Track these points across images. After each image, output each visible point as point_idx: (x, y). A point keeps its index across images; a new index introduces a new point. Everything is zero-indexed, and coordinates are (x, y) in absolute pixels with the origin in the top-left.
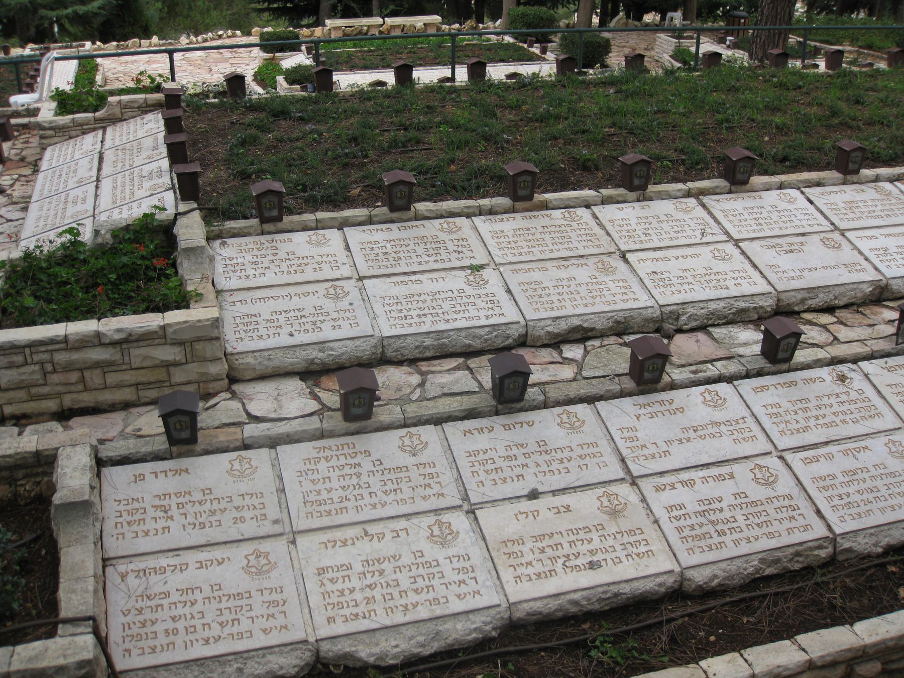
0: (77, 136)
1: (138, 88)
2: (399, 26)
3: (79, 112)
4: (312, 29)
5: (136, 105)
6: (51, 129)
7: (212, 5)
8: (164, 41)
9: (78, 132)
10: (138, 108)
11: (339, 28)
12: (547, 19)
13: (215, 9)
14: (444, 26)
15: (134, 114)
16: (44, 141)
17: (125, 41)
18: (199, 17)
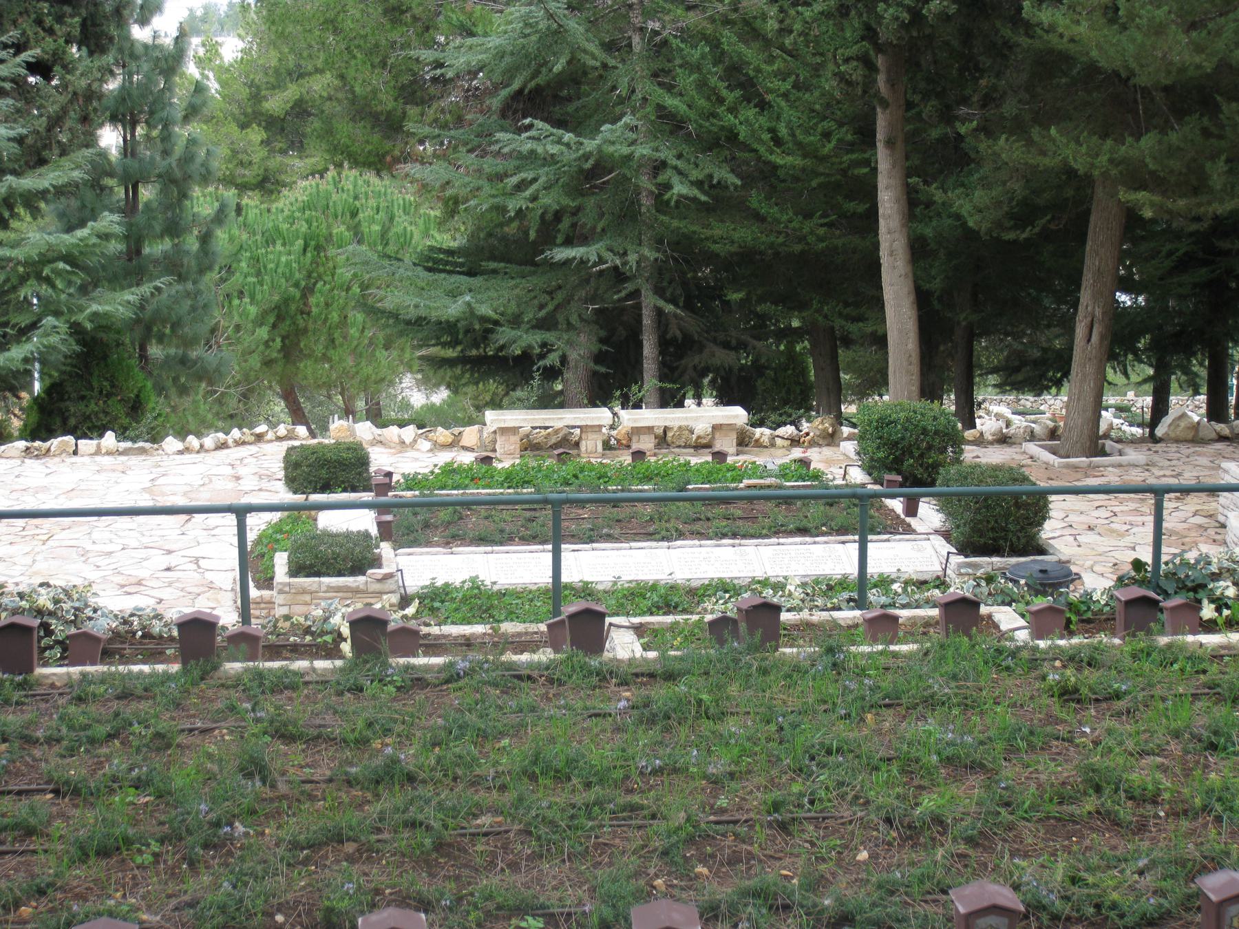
2: (650, 429)
3: (329, 575)
4: (456, 430)
7: (381, 336)
8: (129, 444)
11: (514, 430)
12: (936, 432)
13: (387, 347)
14: (758, 431)
17: (44, 440)
18: (350, 362)
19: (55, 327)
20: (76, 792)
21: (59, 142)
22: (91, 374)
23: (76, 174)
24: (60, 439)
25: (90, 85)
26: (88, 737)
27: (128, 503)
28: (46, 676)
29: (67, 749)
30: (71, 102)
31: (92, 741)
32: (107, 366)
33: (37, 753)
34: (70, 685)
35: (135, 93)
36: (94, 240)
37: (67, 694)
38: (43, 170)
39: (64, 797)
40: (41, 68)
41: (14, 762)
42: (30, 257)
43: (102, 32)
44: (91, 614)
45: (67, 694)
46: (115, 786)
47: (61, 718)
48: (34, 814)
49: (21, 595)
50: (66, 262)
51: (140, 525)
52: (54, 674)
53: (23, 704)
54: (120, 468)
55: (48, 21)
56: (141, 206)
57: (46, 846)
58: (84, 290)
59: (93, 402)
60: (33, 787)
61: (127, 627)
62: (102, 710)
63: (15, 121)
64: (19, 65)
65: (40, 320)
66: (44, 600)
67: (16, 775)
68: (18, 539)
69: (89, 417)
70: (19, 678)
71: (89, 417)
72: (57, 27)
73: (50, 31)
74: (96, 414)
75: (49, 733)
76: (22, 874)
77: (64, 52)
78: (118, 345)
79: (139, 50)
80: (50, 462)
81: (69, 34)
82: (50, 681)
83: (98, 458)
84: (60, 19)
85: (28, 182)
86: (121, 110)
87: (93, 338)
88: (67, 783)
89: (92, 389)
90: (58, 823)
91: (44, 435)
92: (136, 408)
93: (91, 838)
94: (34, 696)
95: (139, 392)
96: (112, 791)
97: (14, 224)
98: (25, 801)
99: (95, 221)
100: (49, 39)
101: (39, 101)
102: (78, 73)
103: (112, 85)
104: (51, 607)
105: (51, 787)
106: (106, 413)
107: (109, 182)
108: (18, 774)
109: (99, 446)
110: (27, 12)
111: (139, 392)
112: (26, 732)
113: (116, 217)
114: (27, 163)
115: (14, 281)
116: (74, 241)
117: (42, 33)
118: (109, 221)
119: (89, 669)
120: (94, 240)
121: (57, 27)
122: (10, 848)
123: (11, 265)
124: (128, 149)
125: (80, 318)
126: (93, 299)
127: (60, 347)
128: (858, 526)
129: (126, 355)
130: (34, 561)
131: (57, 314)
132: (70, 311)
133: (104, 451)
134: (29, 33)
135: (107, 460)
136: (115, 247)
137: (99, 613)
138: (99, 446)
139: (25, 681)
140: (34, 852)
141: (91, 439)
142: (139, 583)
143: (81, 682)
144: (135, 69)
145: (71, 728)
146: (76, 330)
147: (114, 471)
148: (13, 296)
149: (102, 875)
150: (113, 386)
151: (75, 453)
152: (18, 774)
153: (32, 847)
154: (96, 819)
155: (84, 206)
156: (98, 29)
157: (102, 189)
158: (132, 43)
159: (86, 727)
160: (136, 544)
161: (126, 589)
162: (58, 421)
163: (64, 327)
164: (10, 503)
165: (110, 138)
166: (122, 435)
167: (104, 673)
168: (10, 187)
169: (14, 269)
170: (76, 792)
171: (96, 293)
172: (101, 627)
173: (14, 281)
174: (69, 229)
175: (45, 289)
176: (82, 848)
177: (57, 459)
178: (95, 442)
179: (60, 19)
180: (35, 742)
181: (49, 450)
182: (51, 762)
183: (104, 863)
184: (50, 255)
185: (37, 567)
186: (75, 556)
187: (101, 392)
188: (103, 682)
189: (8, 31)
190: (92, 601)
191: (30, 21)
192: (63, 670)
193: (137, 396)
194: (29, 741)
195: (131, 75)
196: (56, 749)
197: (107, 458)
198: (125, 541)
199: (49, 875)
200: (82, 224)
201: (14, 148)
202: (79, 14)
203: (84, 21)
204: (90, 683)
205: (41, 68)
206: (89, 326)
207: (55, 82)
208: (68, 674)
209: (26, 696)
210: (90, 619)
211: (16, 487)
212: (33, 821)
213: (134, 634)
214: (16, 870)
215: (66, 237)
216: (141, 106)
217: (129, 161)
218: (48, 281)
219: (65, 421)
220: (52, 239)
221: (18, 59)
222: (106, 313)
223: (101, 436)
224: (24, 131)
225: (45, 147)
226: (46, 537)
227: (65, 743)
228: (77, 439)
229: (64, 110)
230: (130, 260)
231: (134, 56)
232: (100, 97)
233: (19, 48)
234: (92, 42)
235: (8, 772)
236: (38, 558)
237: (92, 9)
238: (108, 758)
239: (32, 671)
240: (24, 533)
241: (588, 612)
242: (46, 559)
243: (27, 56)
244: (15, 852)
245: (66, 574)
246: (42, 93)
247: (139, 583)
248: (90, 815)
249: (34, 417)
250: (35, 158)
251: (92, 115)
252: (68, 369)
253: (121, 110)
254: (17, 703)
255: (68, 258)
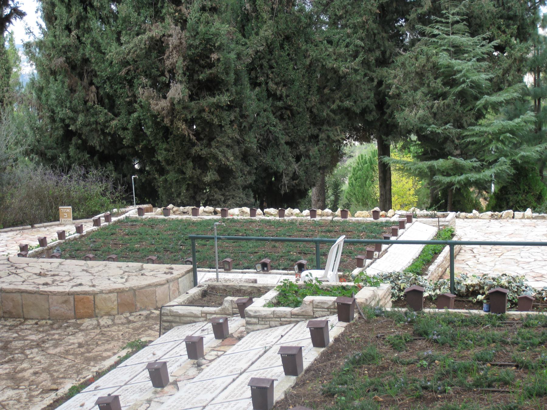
0: (276, 326)
1: (454, 283)
5: (326, 306)
6: (255, 317)
8: (537, 214)
9: (277, 323)
10: (328, 308)
15: (324, 313)
16: (249, 327)
17: (500, 211)
19: (505, 162)
20: (526, 367)
21: (508, 80)
22: (520, 183)
23: (515, 94)
24: (507, 211)
25: (522, 55)
26: (530, 343)
27: (537, 240)
28: (510, 315)
29: (521, 348)
30: (513, 63)
31: (532, 345)
32: (527, 179)
33: (508, 348)
34: (521, 319)
35: (540, 58)
36: (523, 124)
37: (520, 323)
38: (500, 93)
39: (520, 369)
40: (500, 48)
41: (498, 352)
42: (494, 131)
43: (526, 32)
44: (524, 289)
45: (520, 323)
46: (543, 365)
47: (519, 334)
48: (508, 375)
49: (494, 279)
50: (510, 133)
51: (542, 251)
52: (514, 314)
53: (500, 326)
54: (533, 225)
55: (503, 27)
56: (541, 109)
57: (513, 390)
58: (516, 146)
59: (520, 195)
60: (507, 363)
61: (540, 296)
62: (536, 331)
63: (488, 71)
64: (491, 47)
65: (498, 159)
66: (504, 282)
67: (499, 357)
68: (488, 255)
69: (518, 202)
70: (499, 315)
71: (518, 202)
72: (507, 30)
73: (504, 32)
74: (522, 201)
75: (513, 340)
76: (502, 401)
77: (510, 41)
78: (532, 170)
79: (542, 39)
80: (503, 222)
81: (512, 33)
82: (512, 317)
83: (523, 220)
84: (508, 26)
85: (494, 98)
86: (533, 66)
87: (522, 167)
88: (522, 362)
89: (520, 190)
90: (518, 380)
91: (498, 209)
92: (539, 198)
93: (534, 388)
94: (505, 323)
95: (541, 191)
96: (542, 368)
97: (487, 116)
98: (503, 370)
99: (523, 115)
100: (503, 36)
101: (499, 63)
102: (516, 50)
103: (530, 56)
104: (507, 285)
105: (515, 364)
106: (526, 201)
107: (529, 98)
108: (499, 357)
109: (524, 215)
110: (494, 24)
111: (541, 191)
112: (503, 339)
113: (532, 114)
114: (493, 90)
115: (487, 142)
116: (514, 124)
117: (500, 33)
118: (530, 115)
119: (530, 313)
120: (523, 124)
121: (507, 30)
122: (497, 389)
123: (486, 134)
124: (537, 82)
125: (516, 158)
126: (521, 150)
127: (507, 170)
128: (315, 252)
129: (536, 175)
130: (495, 265)
131: (506, 156)
132: (512, 155)
133: (526, 217)
134: (495, 33)
135: (527, 221)
136: (533, 127)
137: (528, 288)
138: (524, 215)
139: (502, 317)
140: (508, 392)
141: (519, 211)
142: (542, 276)
143: (527, 318)
144: (540, 48)
145: (523, 338)
146: (514, 164)
147: (530, 226)
148: (486, 148)
149: (539, 405)
150: (529, 188)
151: (513, 217)
152: (499, 357)
153: (507, 390)
154: (536, 379)
155: (516, 109)
156: (524, 30)
157: (524, 101)
158: (539, 36)
159: (529, 339)
160: (541, 259)
161: (536, 279)
162: (505, 203)
163: (509, 162)
164: (539, 238)
165: (529, 79)
166: (534, 210)
167: (536, 315)
168: (486, 100)
169: (487, 136)
170: (526, 367)
171: (522, 147)
172: (531, 294)
173: (487, 142)
174: (511, 119)
175: (500, 145)
176: (529, 392)
177: (505, 220)
178: (522, 213)
179: (508, 26)
180: (506, 343)
181: (502, 216)
182: (515, 353)
183: (539, 399)
184: (503, 130)
185: (498, 267)
186: (513, 263)
187: (524, 191)
188: (536, 319)
189: (486, 33)
190: (525, 283)
191: (495, 28)
192: (519, 313)
193: (540, 193)
194: (504, 343)
195: (538, 50)
196: (516, 347)
197: (527, 220)
198: (536, 258)
199: (515, 403)
200: (517, 116)
201: (488, 83)
202: (516, 24)
203: (519, 27)
204: (531, 319)
205: (500, 48)
206: (520, 161)
207: (505, 55)
208: (521, 315)
209: (502, 323)
210: (524, 291)
211: (487, 232)
212: (507, 378)
213: (543, 298)
214: (499, 399)
215: (510, 122)
216: (543, 64)
217: (536, 88)
218: (503, 142)
219: (508, 203)
220: (504, 123)
221: (490, 45)
222: (527, 156)
223: (525, 210)
224: (493, 76)
225: (501, 83)
226: (500, 254)
227: (520, 345)
228: (514, 211)
229: (510, 67)
230: (536, 132)
231: (539, 42)
232: (526, 60)
233: (491, 40)
234: (522, 36)
235: (495, 356)
236: (497, 263)
237: (522, 21)
238: (540, 353)
239: (505, 312)
240: (491, 252)
241: (414, 291)
242: (500, 264)
243: (494, 43)
244: (499, 391)
245: (513, 271)
246: (501, 59)
247: (542, 276)
248: (533, 378)
249: (494, 202)
250: (497, 88)
251: (522, 68)
252: (510, 180)
253: (533, 66)
254: (498, 326)
255: (512, 132)
